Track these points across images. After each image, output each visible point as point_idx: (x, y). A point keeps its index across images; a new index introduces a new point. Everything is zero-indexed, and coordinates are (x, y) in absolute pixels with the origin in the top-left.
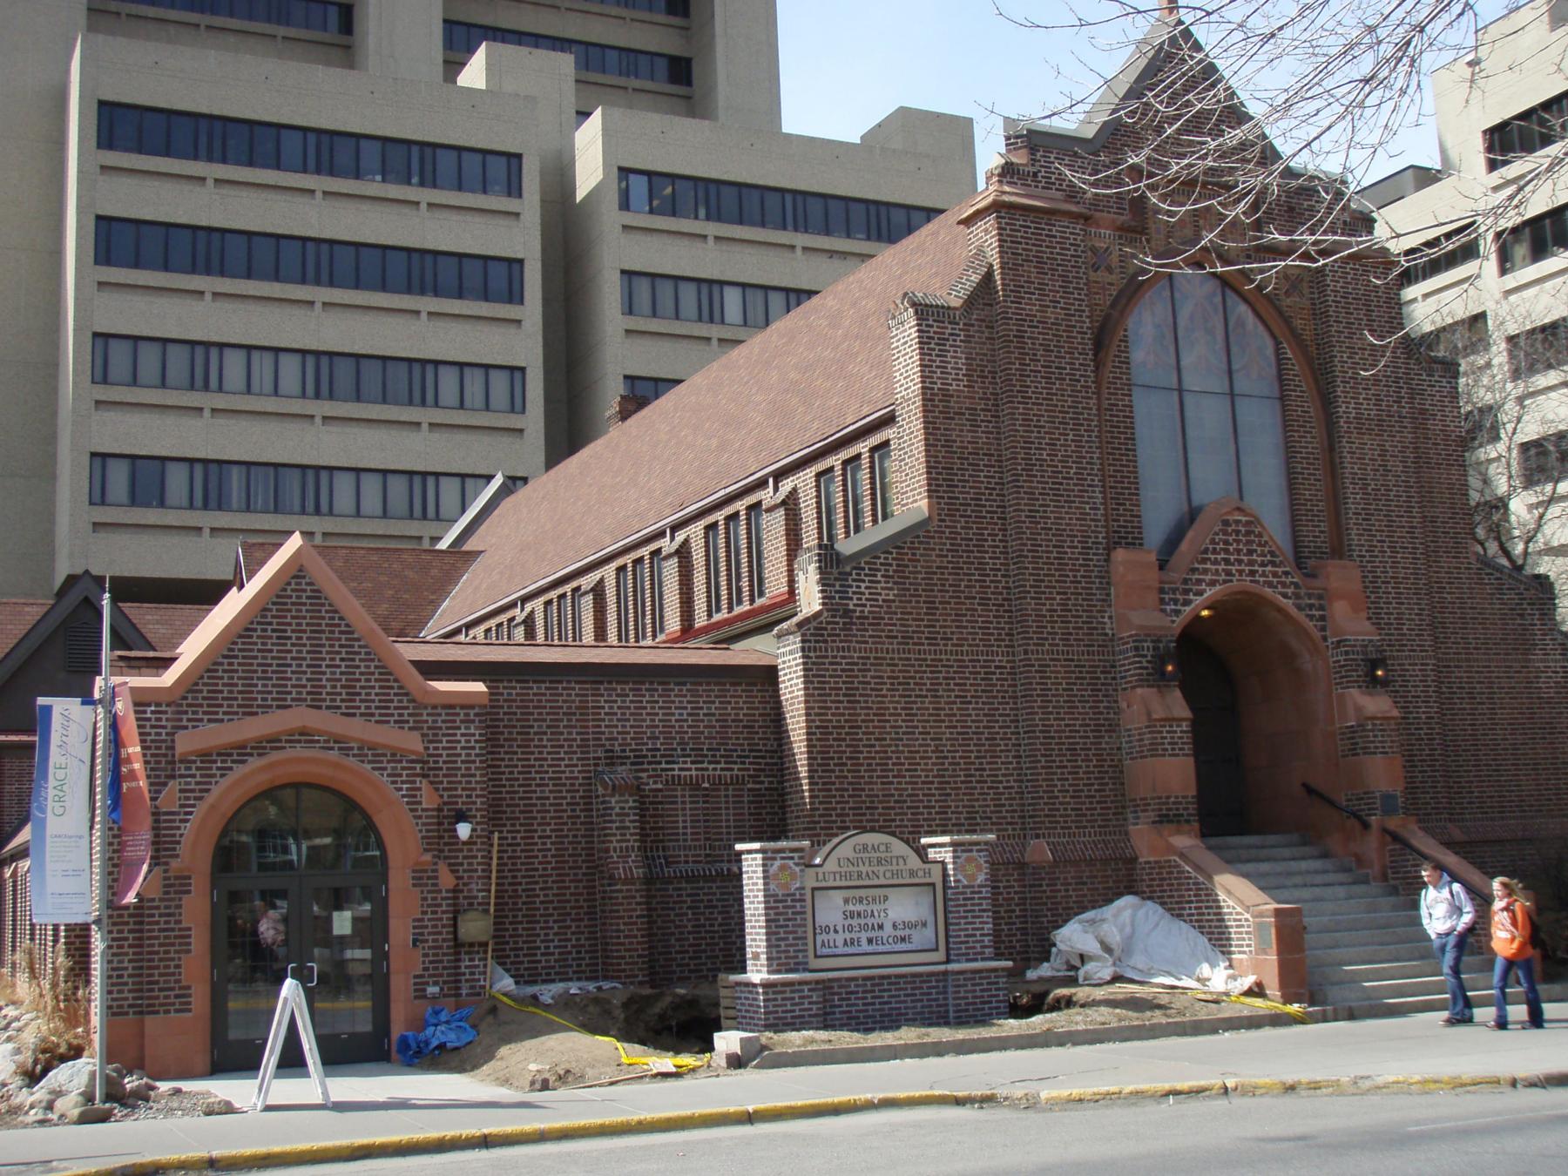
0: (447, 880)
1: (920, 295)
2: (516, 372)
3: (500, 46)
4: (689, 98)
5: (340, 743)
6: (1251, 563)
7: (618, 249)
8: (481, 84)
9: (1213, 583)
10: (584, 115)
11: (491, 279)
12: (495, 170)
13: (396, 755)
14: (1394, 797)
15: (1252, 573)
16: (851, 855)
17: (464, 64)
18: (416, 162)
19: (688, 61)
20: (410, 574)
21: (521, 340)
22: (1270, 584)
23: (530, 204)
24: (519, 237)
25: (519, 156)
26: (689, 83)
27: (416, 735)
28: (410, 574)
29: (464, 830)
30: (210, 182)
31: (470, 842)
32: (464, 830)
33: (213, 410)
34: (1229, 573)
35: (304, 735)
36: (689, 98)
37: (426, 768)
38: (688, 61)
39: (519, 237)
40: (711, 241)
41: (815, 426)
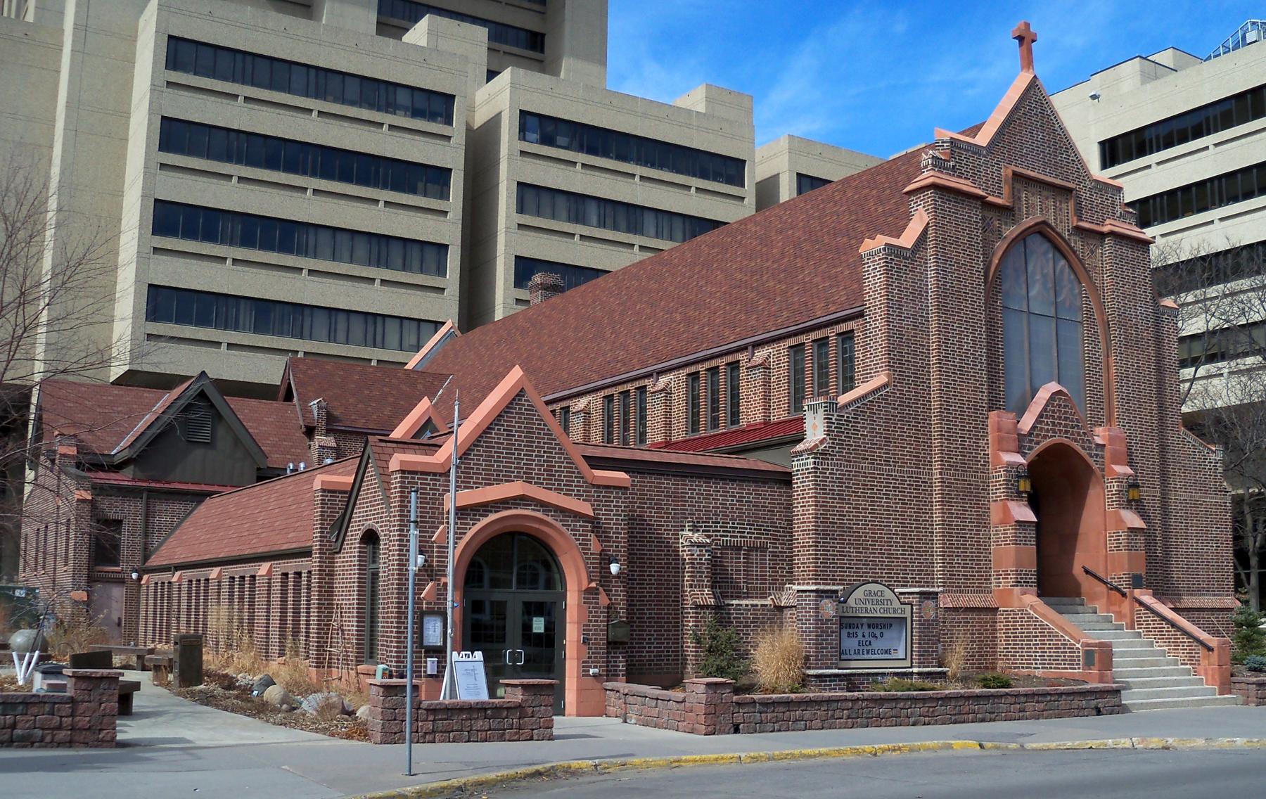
0: (603, 600)
1: (1051, 255)
2: (443, 248)
3: (439, 19)
4: (541, 61)
5: (544, 505)
6: (1066, 426)
7: (512, 166)
8: (423, 42)
9: (1045, 437)
10: (491, 74)
11: (432, 179)
12: (436, 105)
13: (577, 515)
14: (1140, 576)
15: (1067, 432)
16: (862, 597)
17: (408, 30)
18: (378, 93)
19: (543, 36)
20: (404, 387)
21: (444, 226)
22: (1076, 440)
23: (457, 130)
24: (451, 156)
25: (453, 97)
26: (542, 51)
27: (588, 504)
28: (404, 387)
29: (614, 568)
30: (241, 99)
31: (618, 576)
32: (614, 568)
33: (234, 260)
34: (1054, 431)
35: (522, 500)
36: (541, 61)
37: (594, 524)
38: (543, 36)
39: (451, 156)
40: (579, 166)
41: (785, 314)
